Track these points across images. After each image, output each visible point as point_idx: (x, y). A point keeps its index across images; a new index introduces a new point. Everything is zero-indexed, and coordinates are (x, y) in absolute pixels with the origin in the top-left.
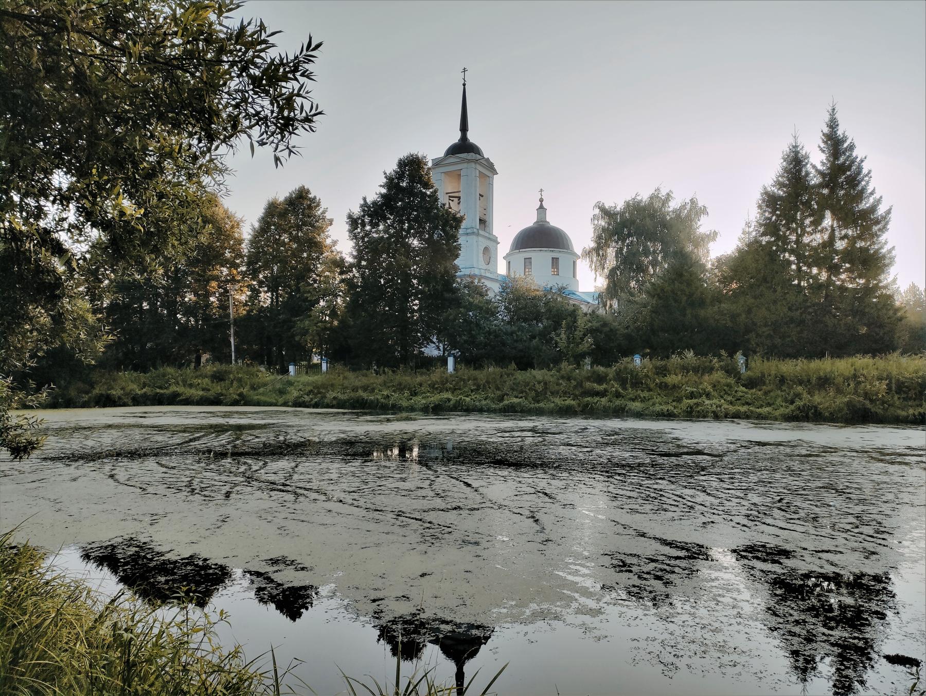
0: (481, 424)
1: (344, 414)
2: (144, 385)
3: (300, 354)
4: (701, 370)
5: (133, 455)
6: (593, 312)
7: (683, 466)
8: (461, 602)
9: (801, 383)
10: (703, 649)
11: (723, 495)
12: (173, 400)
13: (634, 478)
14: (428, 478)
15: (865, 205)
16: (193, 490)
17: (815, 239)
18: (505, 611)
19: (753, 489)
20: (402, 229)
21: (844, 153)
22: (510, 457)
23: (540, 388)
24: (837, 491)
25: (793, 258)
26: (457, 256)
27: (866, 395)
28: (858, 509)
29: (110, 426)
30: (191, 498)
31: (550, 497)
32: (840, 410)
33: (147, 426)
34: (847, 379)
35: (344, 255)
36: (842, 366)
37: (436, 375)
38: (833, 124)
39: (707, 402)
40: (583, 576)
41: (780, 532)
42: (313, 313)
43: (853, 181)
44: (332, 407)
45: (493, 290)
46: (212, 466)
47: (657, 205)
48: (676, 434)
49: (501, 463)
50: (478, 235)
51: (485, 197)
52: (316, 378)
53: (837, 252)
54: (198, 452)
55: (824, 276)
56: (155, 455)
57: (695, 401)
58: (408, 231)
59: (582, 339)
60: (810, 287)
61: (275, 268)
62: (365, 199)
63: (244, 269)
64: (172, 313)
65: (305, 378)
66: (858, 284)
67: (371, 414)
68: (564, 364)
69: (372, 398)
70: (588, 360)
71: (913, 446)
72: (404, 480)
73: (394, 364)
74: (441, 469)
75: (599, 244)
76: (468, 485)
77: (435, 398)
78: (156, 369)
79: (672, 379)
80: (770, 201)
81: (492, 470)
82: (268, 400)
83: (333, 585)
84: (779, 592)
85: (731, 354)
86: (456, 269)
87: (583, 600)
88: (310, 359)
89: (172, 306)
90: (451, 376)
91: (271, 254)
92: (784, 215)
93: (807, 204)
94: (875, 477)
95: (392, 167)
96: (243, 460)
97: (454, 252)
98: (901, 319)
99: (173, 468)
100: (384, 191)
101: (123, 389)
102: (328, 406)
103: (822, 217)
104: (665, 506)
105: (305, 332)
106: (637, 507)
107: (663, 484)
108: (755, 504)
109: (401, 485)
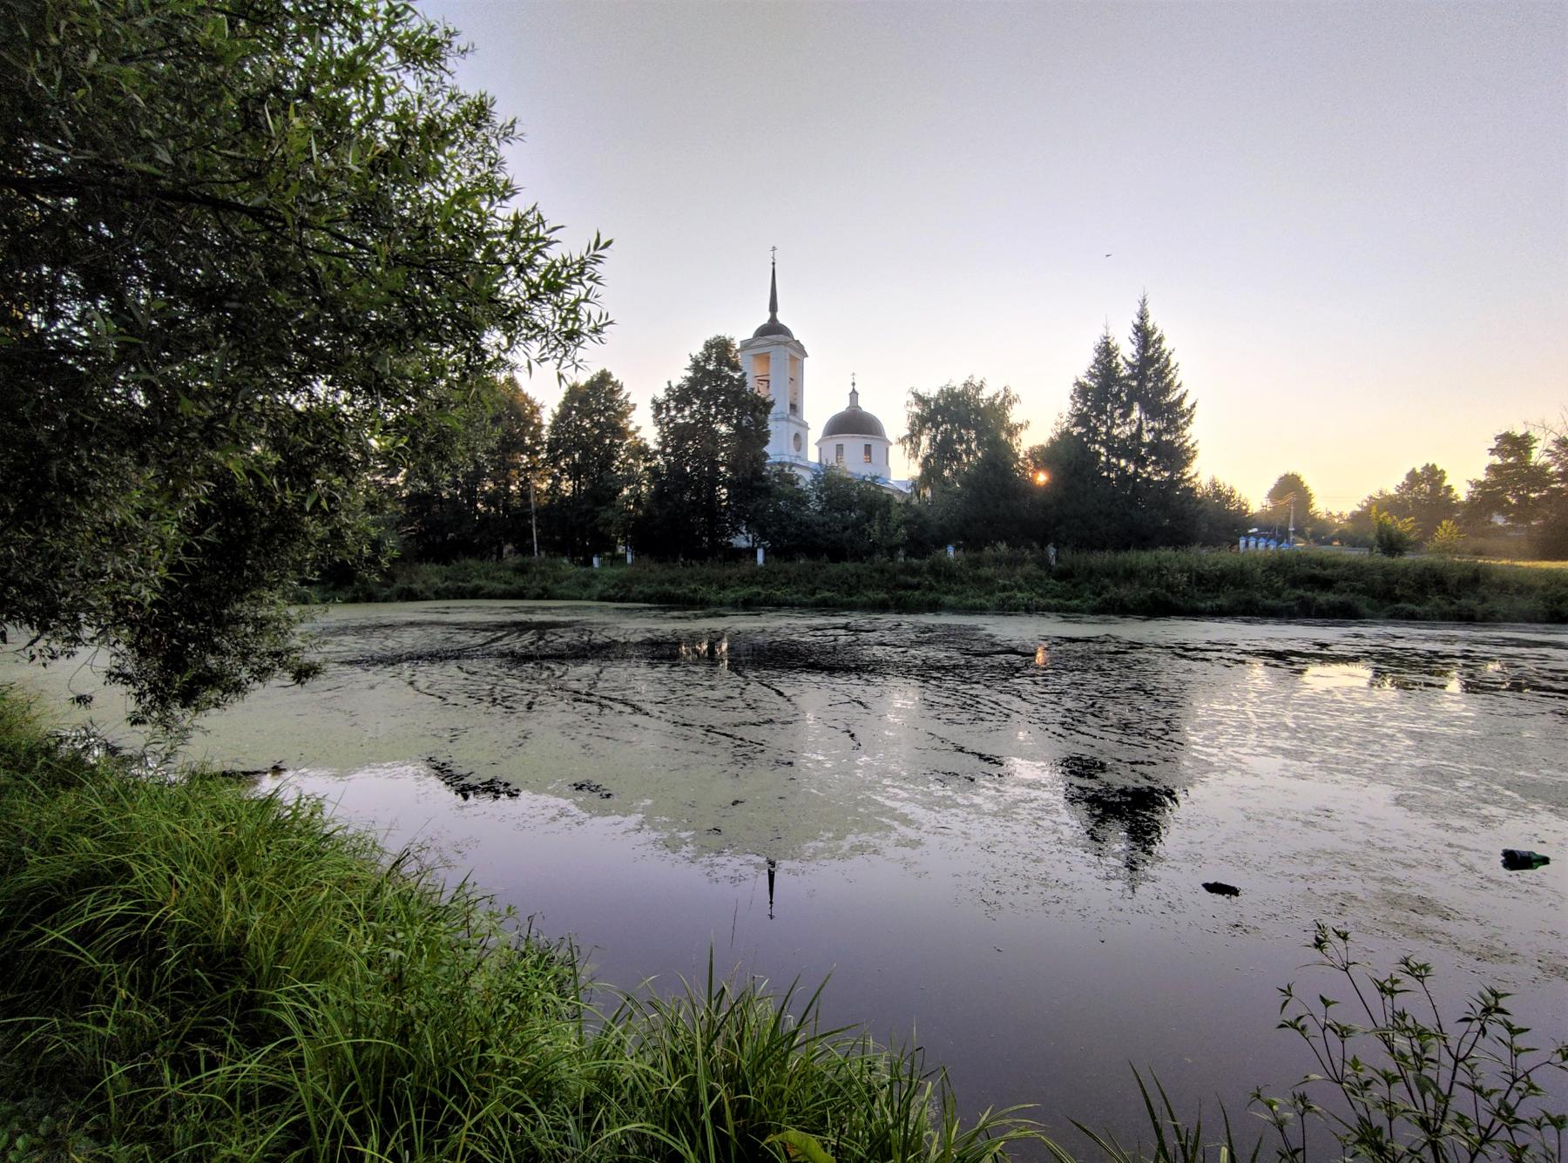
0: (792, 621)
1: (650, 609)
2: (447, 578)
3: (603, 544)
4: (1013, 562)
5: (435, 657)
6: (907, 502)
7: (997, 668)
8: (775, 834)
9: (1108, 575)
10: (1025, 883)
11: (1037, 700)
12: (475, 594)
13: (950, 683)
14: (738, 687)
15: (1173, 397)
16: (495, 700)
17: (1124, 431)
18: (821, 844)
19: (1066, 692)
20: (709, 414)
21: (1153, 345)
22: (827, 660)
23: (853, 581)
24: (1146, 692)
25: (1102, 450)
26: (766, 443)
27: (1169, 587)
28: (1167, 712)
29: (412, 624)
30: (492, 710)
31: (866, 708)
32: (1144, 602)
33: (450, 624)
34: (1151, 572)
35: (647, 442)
36: (1145, 558)
37: (745, 568)
38: (1143, 317)
39: (1019, 595)
40: (902, 800)
41: (1093, 741)
42: (617, 503)
43: (1161, 374)
44: (638, 601)
45: (805, 478)
46: (514, 672)
47: (972, 392)
48: (990, 630)
49: (814, 667)
50: (788, 420)
51: (796, 381)
52: (621, 570)
53: (1144, 445)
54: (502, 655)
55: (1131, 468)
56: (457, 658)
57: (1007, 594)
58: (715, 418)
59: (896, 530)
60: (1118, 478)
61: (577, 456)
62: (669, 383)
63: (544, 456)
64: (472, 503)
65: (615, 571)
66: (1163, 476)
67: (678, 609)
68: (877, 557)
69: (679, 592)
70: (901, 552)
71: (1213, 640)
72: (712, 688)
73: (701, 556)
74: (751, 675)
75: (912, 431)
76: (780, 694)
77: (744, 592)
78: (458, 561)
79: (986, 571)
80: (1082, 391)
81: (805, 675)
82: (571, 593)
83: (640, 816)
84: (1097, 812)
85: (1043, 546)
86: (766, 456)
87: (902, 829)
88: (614, 549)
89: (470, 494)
90: (761, 568)
91: (573, 441)
92: (1095, 407)
93: (1117, 396)
94: (1179, 676)
95: (698, 350)
96: (546, 664)
97: (763, 438)
98: (1202, 511)
99: (475, 673)
100: (690, 374)
101: (424, 582)
102: (634, 601)
103: (1131, 409)
104: (982, 715)
105: (608, 523)
106: (954, 716)
107: (979, 689)
108: (1068, 710)
109: (710, 693)
